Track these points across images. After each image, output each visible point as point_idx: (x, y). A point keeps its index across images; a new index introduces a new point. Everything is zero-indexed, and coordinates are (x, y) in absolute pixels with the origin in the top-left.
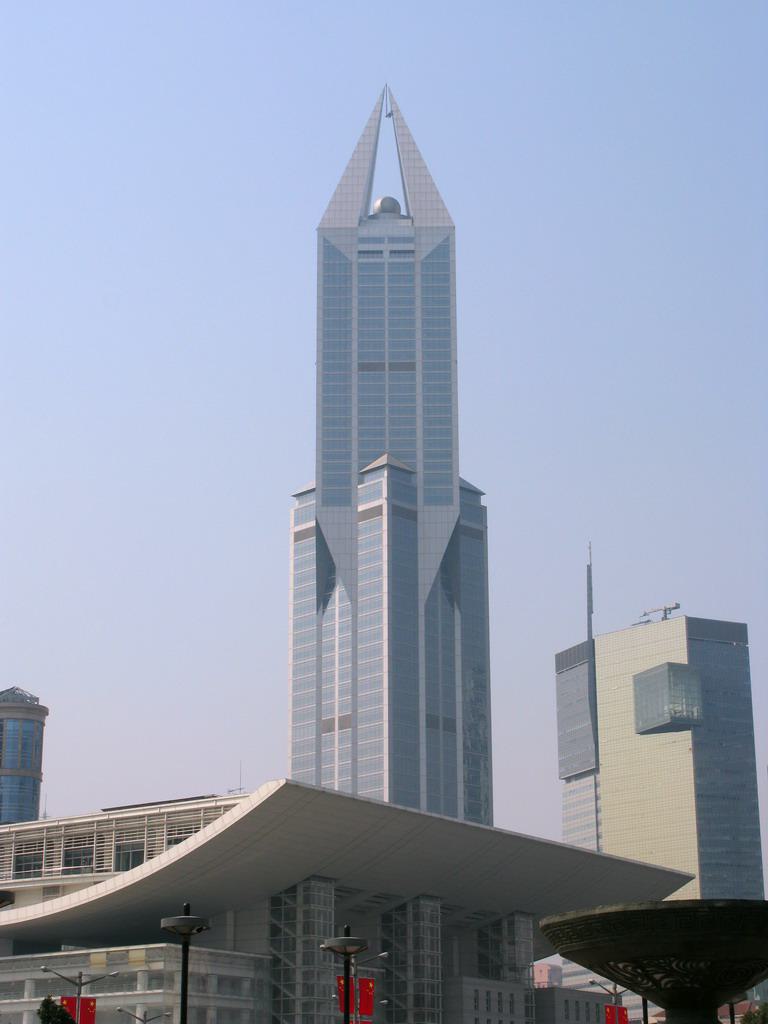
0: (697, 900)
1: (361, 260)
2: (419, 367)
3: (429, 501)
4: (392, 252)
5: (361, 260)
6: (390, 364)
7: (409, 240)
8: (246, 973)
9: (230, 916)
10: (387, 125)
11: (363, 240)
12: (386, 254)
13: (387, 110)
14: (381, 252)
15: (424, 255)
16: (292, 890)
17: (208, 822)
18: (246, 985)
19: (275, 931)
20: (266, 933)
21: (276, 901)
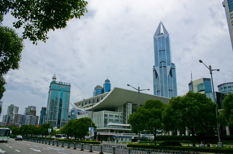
3: (168, 65)
7: (164, 36)
9: (119, 108)
10: (161, 25)
13: (161, 23)
16: (126, 104)
17: (106, 95)
19: (124, 109)
21: (124, 106)
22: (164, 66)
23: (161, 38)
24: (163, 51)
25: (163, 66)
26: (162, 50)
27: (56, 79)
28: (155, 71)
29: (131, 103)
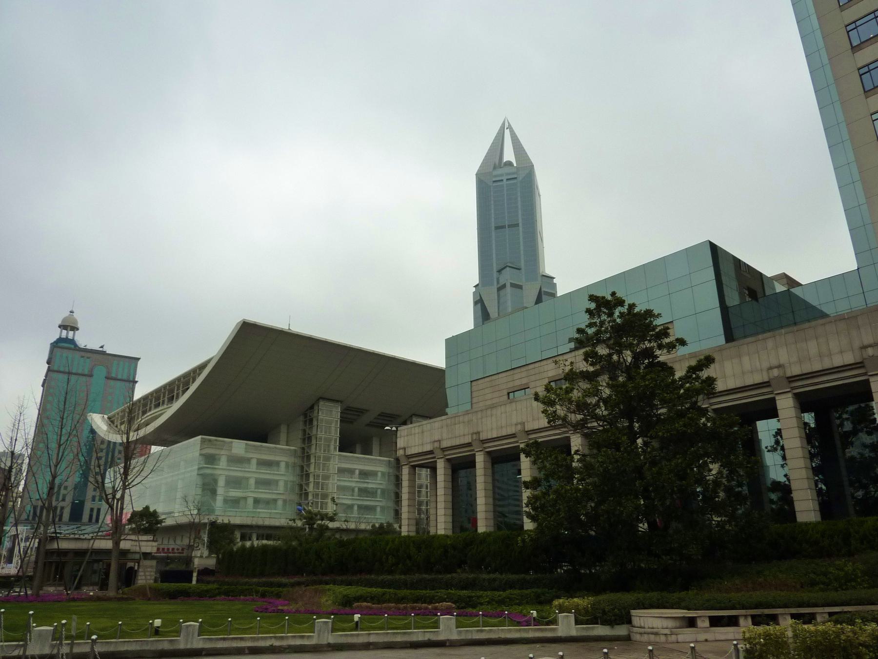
0: (843, 277)
1: (494, 185)
2: (520, 225)
4: (507, 180)
5: (494, 185)
6: (508, 225)
8: (283, 459)
10: (507, 133)
11: (495, 176)
12: (505, 180)
14: (502, 180)
15: (521, 178)
17: (199, 375)
18: (283, 465)
20: (300, 435)
22: (513, 285)
23: (504, 178)
24: (509, 226)
25: (508, 285)
26: (507, 223)
27: (74, 329)
28: (479, 305)
29: (337, 401)
